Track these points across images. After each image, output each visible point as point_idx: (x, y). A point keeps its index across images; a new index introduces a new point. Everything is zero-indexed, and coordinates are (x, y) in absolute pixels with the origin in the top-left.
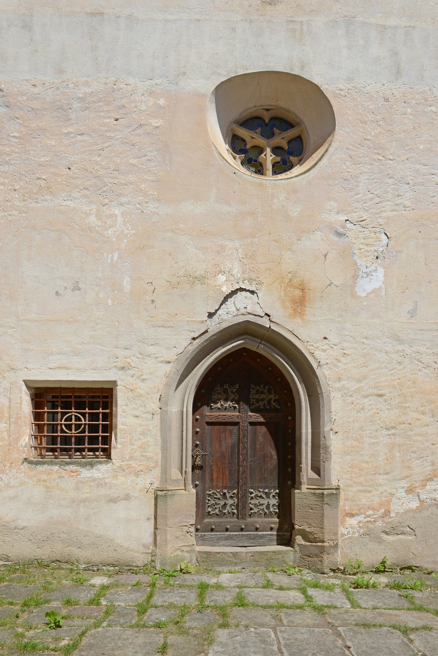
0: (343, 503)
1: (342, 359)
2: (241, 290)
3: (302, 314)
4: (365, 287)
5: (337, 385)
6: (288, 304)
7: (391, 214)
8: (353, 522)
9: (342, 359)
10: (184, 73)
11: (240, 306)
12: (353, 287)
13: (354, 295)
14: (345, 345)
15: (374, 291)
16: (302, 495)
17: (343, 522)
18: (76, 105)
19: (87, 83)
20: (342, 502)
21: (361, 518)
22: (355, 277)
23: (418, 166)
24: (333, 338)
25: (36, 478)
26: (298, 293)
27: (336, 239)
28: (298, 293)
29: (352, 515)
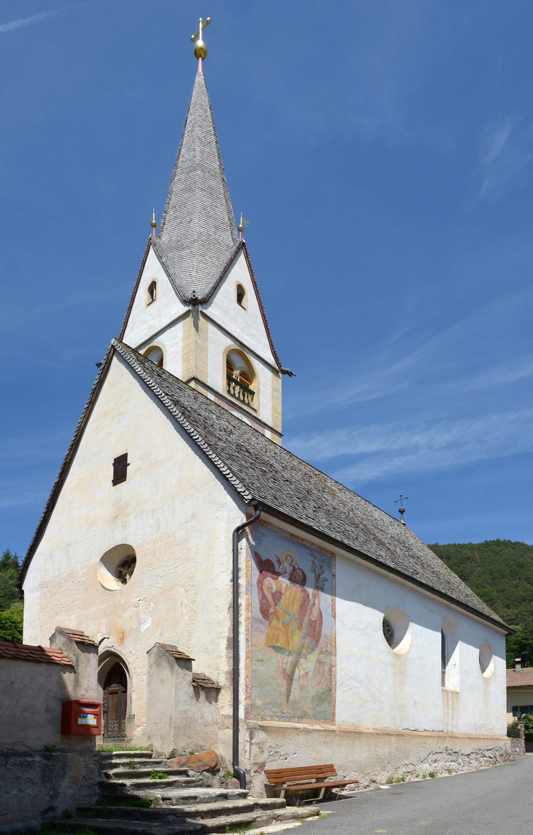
0: (136, 722)
1: (136, 660)
2: (105, 638)
3: (123, 644)
4: (144, 627)
5: (135, 671)
6: (119, 641)
7: (155, 593)
8: (139, 729)
9: (136, 660)
10: (194, 292)
11: (105, 644)
12: (139, 628)
13: (140, 632)
14: (138, 653)
15: (147, 628)
16: (482, 737)
17: (136, 729)
18: (63, 581)
19: (66, 572)
20: (135, 721)
21: (141, 727)
22: (140, 624)
23: (165, 568)
24: (133, 652)
25: (259, 716)
26: (122, 635)
27: (135, 609)
28: (122, 635)
29: (139, 726)
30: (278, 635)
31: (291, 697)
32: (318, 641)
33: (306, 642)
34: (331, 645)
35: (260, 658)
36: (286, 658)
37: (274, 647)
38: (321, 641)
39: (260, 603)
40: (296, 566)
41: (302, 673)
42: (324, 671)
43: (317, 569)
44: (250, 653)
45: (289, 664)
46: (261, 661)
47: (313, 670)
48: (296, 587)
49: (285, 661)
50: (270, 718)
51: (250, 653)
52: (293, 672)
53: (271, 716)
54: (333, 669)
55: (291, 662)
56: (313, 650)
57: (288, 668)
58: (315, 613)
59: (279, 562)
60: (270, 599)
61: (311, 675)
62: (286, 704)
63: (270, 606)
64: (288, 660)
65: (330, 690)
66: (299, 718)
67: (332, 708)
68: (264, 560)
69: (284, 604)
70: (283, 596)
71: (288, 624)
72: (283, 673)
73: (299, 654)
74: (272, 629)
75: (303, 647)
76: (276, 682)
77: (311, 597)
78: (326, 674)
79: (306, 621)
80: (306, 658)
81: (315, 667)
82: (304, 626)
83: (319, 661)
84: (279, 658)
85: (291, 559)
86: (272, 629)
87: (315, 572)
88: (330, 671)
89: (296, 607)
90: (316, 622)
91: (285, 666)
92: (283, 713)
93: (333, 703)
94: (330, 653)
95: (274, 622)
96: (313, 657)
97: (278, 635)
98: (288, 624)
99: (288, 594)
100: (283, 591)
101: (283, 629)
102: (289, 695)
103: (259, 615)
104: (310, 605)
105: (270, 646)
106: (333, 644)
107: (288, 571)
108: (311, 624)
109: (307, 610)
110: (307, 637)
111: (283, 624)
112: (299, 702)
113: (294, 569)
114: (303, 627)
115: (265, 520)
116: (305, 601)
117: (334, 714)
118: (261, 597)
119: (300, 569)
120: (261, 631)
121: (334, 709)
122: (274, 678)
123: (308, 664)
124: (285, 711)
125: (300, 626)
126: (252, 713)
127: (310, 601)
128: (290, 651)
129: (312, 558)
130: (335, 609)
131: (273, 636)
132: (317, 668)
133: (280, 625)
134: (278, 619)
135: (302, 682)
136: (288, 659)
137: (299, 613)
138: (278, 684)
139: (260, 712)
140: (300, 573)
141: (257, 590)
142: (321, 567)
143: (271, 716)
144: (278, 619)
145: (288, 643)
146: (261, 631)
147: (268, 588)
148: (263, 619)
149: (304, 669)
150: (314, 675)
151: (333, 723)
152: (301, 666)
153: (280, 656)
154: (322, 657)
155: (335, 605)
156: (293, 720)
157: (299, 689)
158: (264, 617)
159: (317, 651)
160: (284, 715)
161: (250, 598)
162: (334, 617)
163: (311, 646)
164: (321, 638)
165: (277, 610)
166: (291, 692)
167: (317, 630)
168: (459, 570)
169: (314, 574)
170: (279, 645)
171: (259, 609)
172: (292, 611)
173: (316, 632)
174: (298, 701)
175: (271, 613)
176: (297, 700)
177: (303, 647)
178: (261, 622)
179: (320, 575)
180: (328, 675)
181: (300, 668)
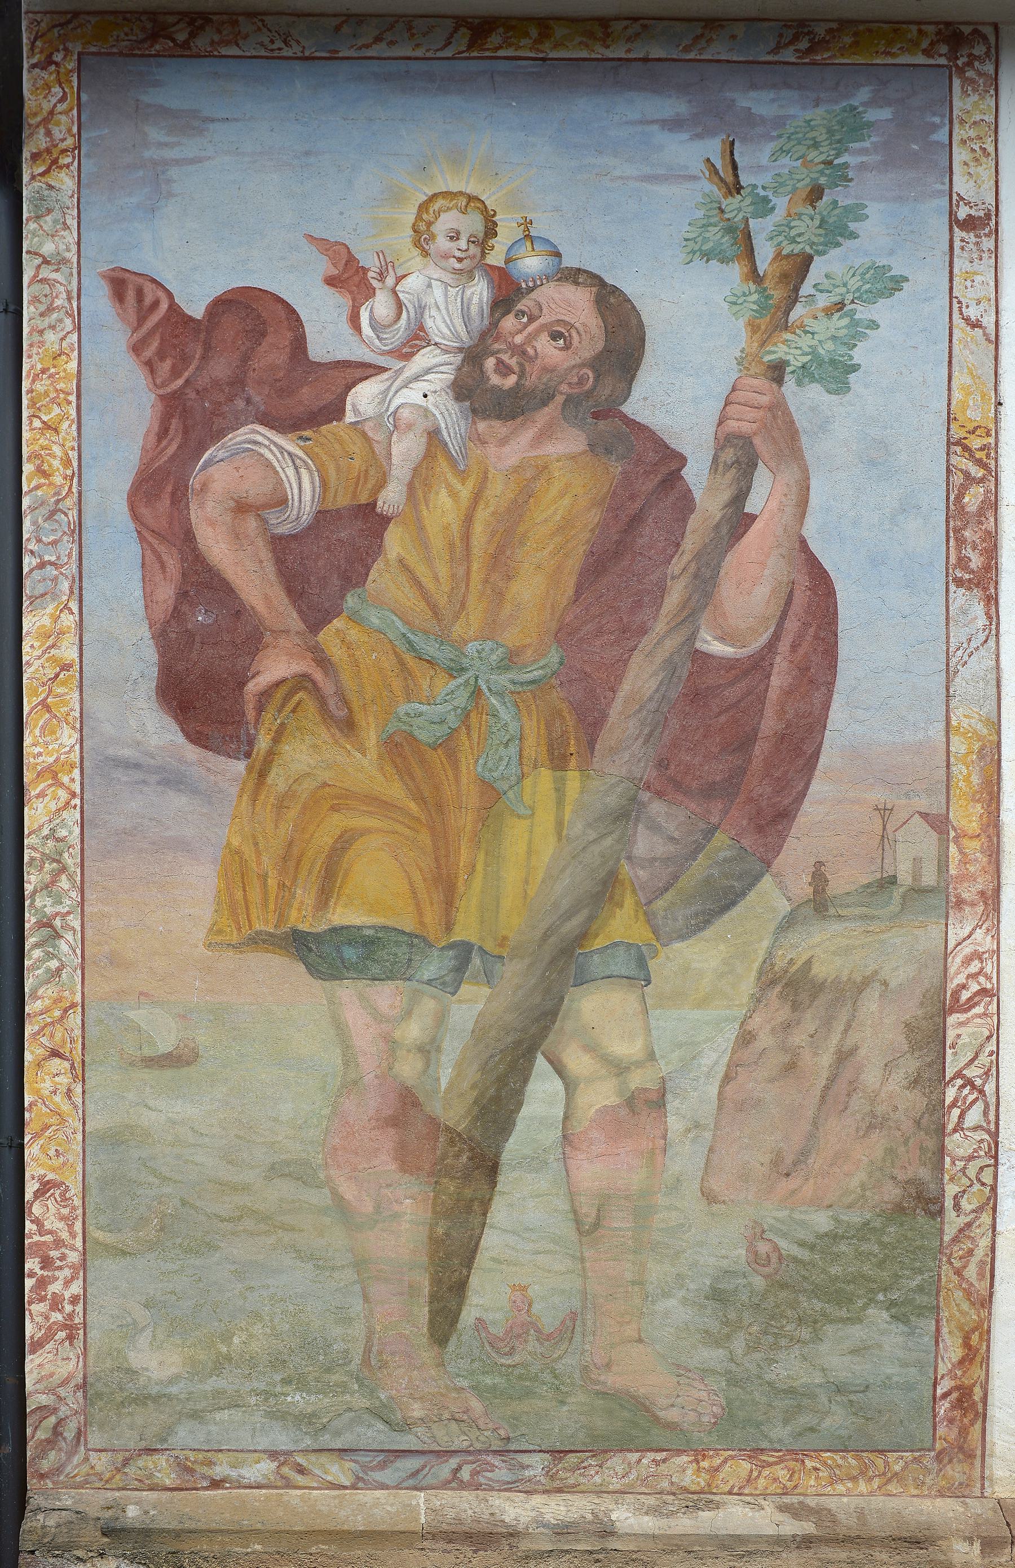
30: (344, 842)
31: (485, 1299)
32: (775, 819)
33: (644, 843)
34: (939, 824)
35: (165, 1044)
36: (428, 1005)
37: (299, 944)
38: (810, 811)
39: (161, 636)
40: (531, 264)
41: (600, 1096)
42: (844, 1056)
43: (761, 229)
44: (74, 1019)
45: (452, 1049)
46: (174, 1060)
47: (715, 1056)
48: (528, 435)
49: (413, 1031)
50: (266, 1467)
51: (74, 1019)
52: (498, 1105)
53: (273, 1455)
54: (962, 1030)
55: (479, 1033)
56: (721, 900)
57: (449, 1084)
58: (751, 590)
59: (350, 279)
60: (255, 583)
61: (695, 1099)
62: (427, 1355)
63: (253, 641)
64: (433, 1031)
65: (929, 1203)
66: (558, 1454)
67: (952, 1350)
68: (197, 310)
69: (406, 596)
70: (395, 542)
71: (448, 745)
72: (395, 1122)
73: (565, 960)
74: (281, 806)
75: (605, 890)
76: (319, 1198)
77: (696, 474)
78: (871, 1077)
79: (643, 678)
80: (640, 975)
81: (745, 1038)
82: (623, 723)
83: (792, 987)
84: (355, 1016)
85: (472, 224)
86: (281, 806)
87: (749, 253)
88: (930, 1038)
89: (537, 589)
90: (758, 665)
91: (408, 1069)
92: (405, 1426)
93: (956, 1308)
94: (918, 891)
95: (305, 755)
96: (712, 969)
97: (344, 842)
98: (448, 745)
99: (444, 507)
100: (391, 497)
101: (396, 791)
102: (460, 1288)
103: (159, 732)
104: (690, 543)
105: (258, 941)
106: (967, 816)
107: (437, 325)
108: (696, 696)
109: (661, 590)
110: (657, 808)
111: (400, 750)
112: (569, 1327)
113: (508, 291)
114: (606, 739)
115: (950, 19)
116: (636, 520)
117: (970, 1404)
118: (166, 593)
119: (574, 276)
120: (182, 845)
121: (976, 1351)
122: (299, 1172)
123: (674, 1019)
124: (417, 1411)
125: (577, 729)
126: (95, 1438)
127: (686, 504)
128: (464, 951)
129: (713, 148)
130: (992, 504)
131: (290, 859)
132: (765, 1040)
133: (362, 766)
134: (348, 726)
135: (591, 1172)
136: (441, 1018)
137: (565, 634)
138: (341, 1207)
139: (169, 1430)
140: (576, 305)
141: (133, 550)
142: (815, 194)
143: (273, 1455)
144: (348, 726)
145: (447, 888)
146: (182, 845)
147: (241, 508)
148: (192, 752)
149: (620, 1068)
150: (732, 1104)
151: (956, 1472)
152: (592, 1048)
153: (363, 1005)
154: (826, 949)
155: (992, 473)
156: (502, 1473)
157: (567, 1230)
158: (197, 738)
159: (770, 898)
160: (407, 1441)
161: (69, 620)
162: (983, 580)
163: (699, 868)
164: (818, 787)
165: (336, 652)
166: (482, 1259)
167: (769, 724)
168: (336, 581)
169: (735, 271)
170: (342, 915)
171: (149, 685)
172: (490, 630)
173: (760, 750)
174: (549, 1323)
175: (266, 695)
176: (548, 1314)
177: (605, 890)
178: (172, 780)
179: (805, 263)
180: (897, 1081)
181: (578, 1061)
